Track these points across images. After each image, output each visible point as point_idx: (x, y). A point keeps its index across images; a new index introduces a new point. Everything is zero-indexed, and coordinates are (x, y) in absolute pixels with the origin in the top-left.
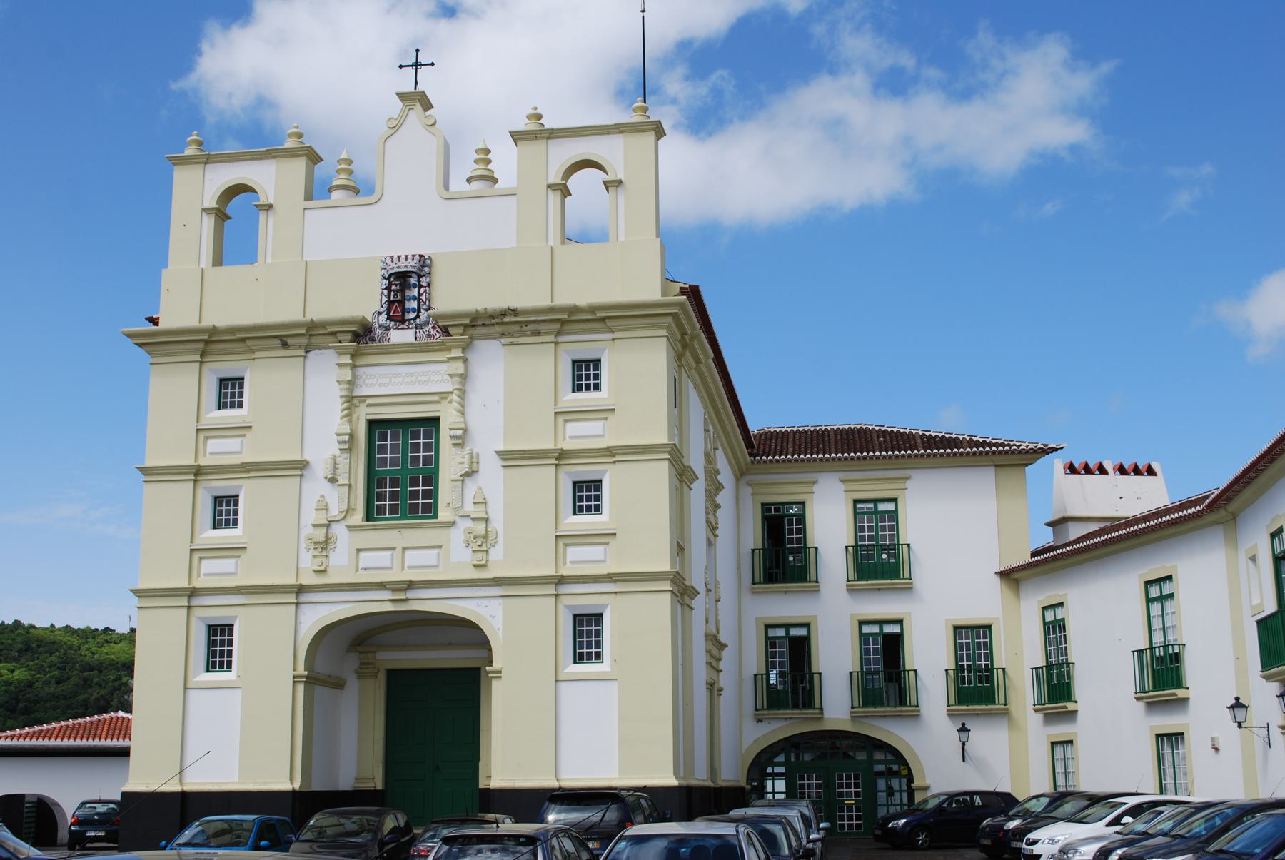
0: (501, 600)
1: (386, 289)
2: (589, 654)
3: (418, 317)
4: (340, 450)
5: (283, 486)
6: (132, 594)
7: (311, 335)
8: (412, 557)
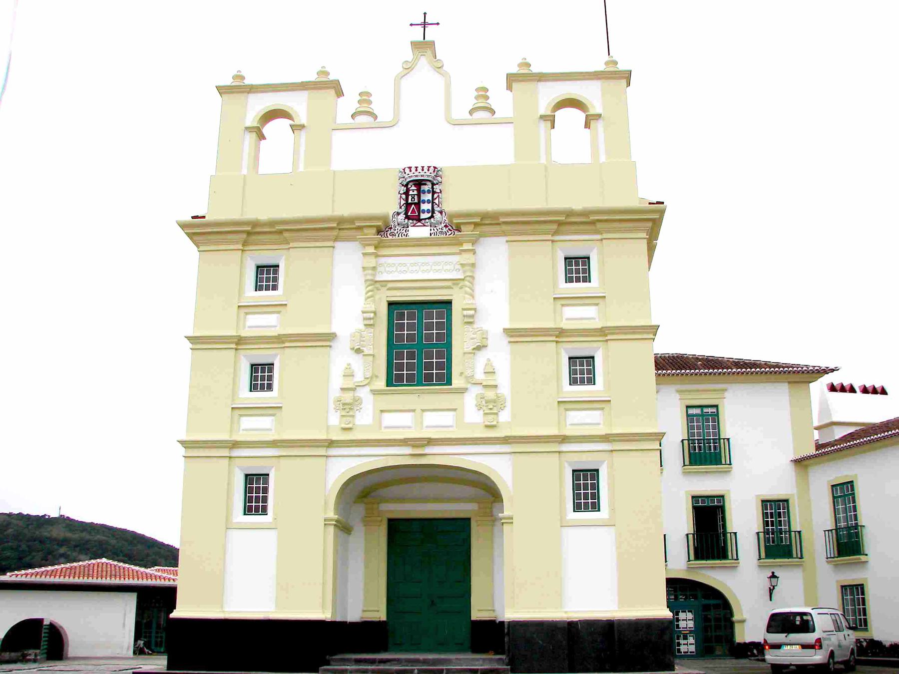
0: (508, 456)
1: (404, 193)
2: (586, 504)
3: (432, 216)
4: (365, 325)
5: (309, 356)
6: (180, 445)
7: (340, 229)
8: (431, 418)
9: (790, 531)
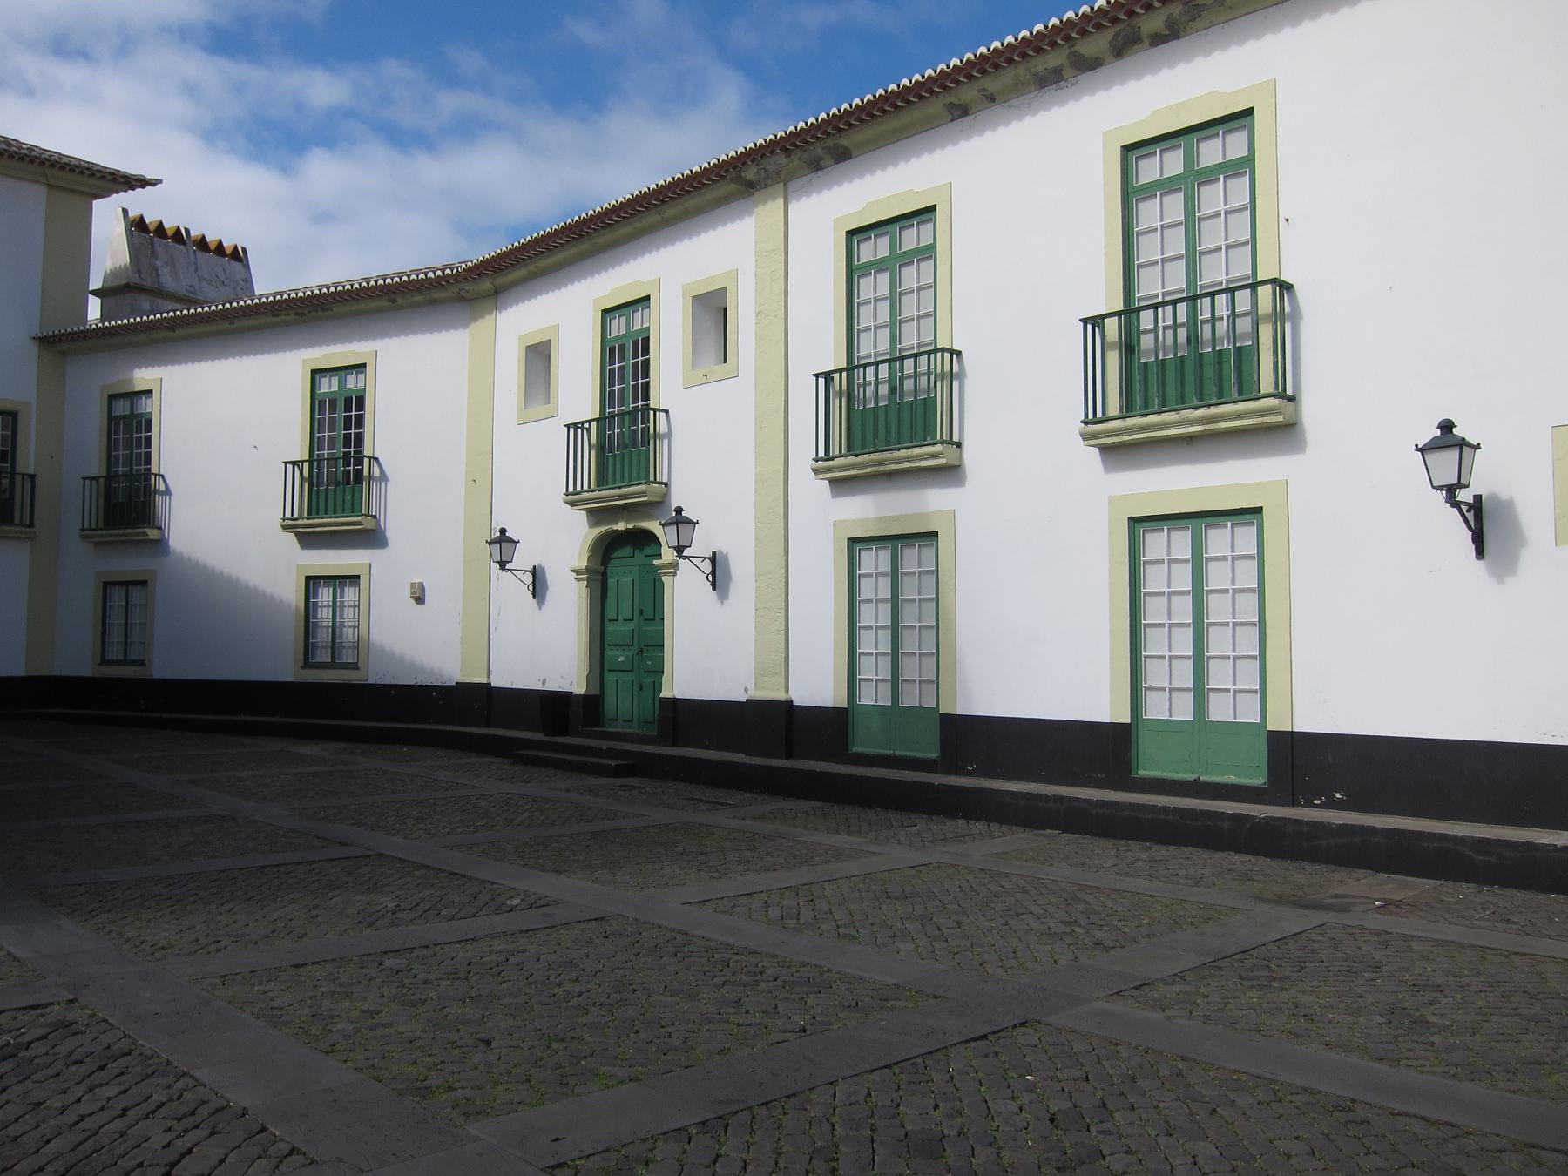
9: (13, 473)
